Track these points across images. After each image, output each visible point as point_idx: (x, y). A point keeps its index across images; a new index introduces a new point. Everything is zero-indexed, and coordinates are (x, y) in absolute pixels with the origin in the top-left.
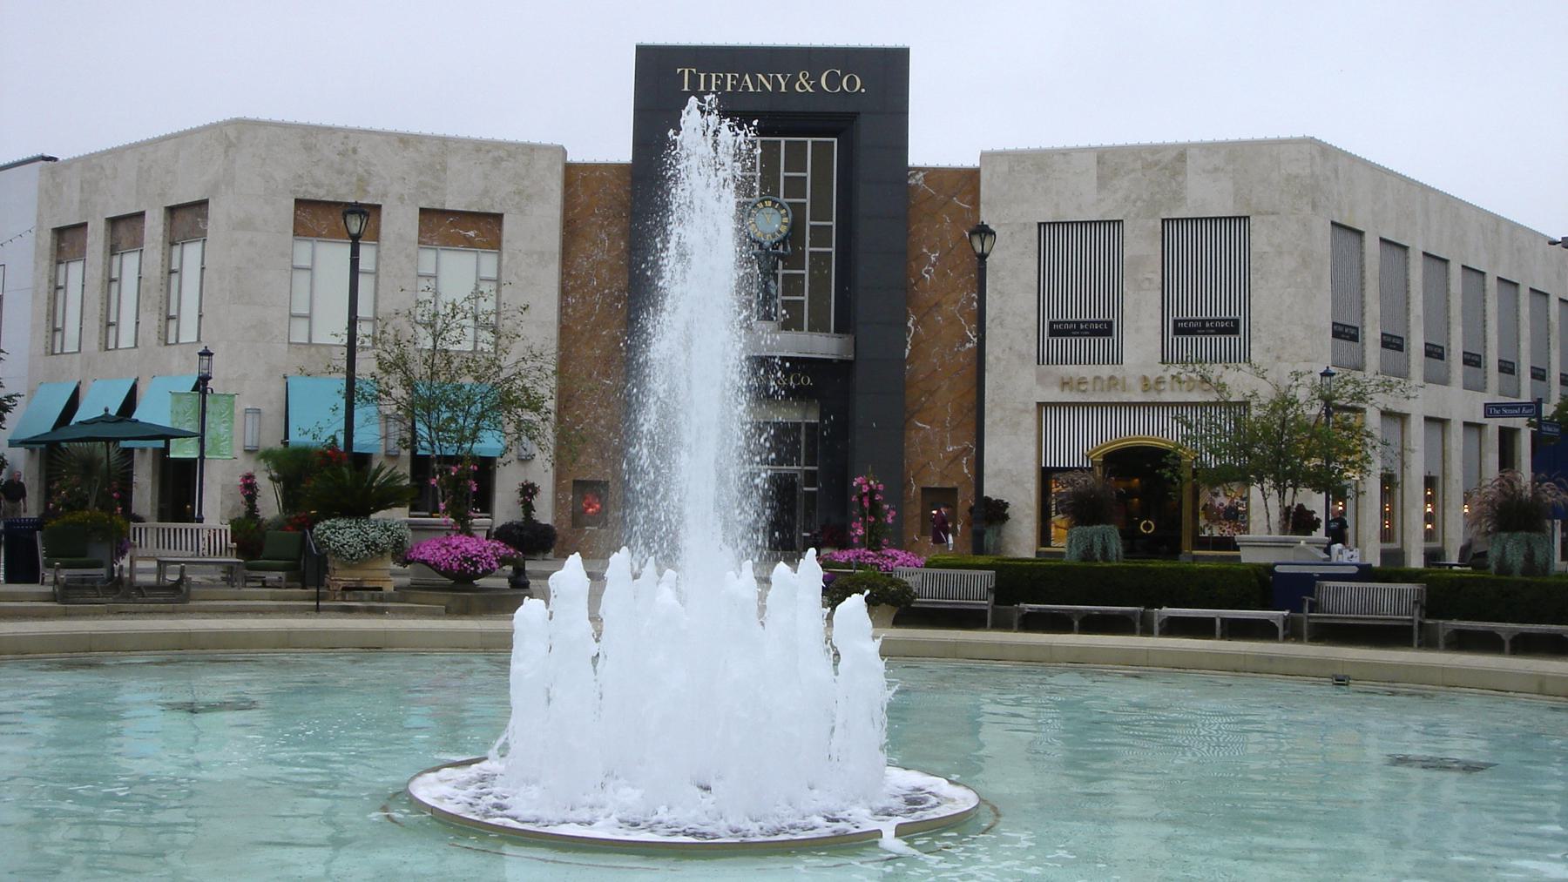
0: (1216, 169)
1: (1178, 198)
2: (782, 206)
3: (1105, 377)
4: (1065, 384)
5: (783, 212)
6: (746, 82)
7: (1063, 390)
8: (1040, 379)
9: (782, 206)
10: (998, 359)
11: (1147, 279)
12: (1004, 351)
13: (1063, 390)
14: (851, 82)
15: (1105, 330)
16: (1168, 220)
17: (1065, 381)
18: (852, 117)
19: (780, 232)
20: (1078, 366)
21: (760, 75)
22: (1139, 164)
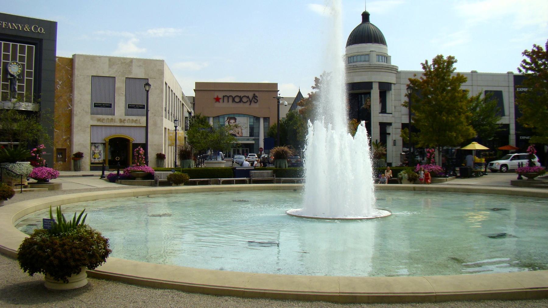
0: (140, 66)
1: (130, 72)
2: (19, 65)
3: (110, 119)
4: (99, 120)
5: (20, 66)
6: (9, 25)
8: (92, 119)
9: (19, 65)
10: (80, 113)
12: (81, 111)
14: (41, 30)
15: (109, 106)
16: (127, 78)
17: (99, 119)
18: (41, 40)
19: (18, 72)
21: (14, 24)
22: (120, 63)
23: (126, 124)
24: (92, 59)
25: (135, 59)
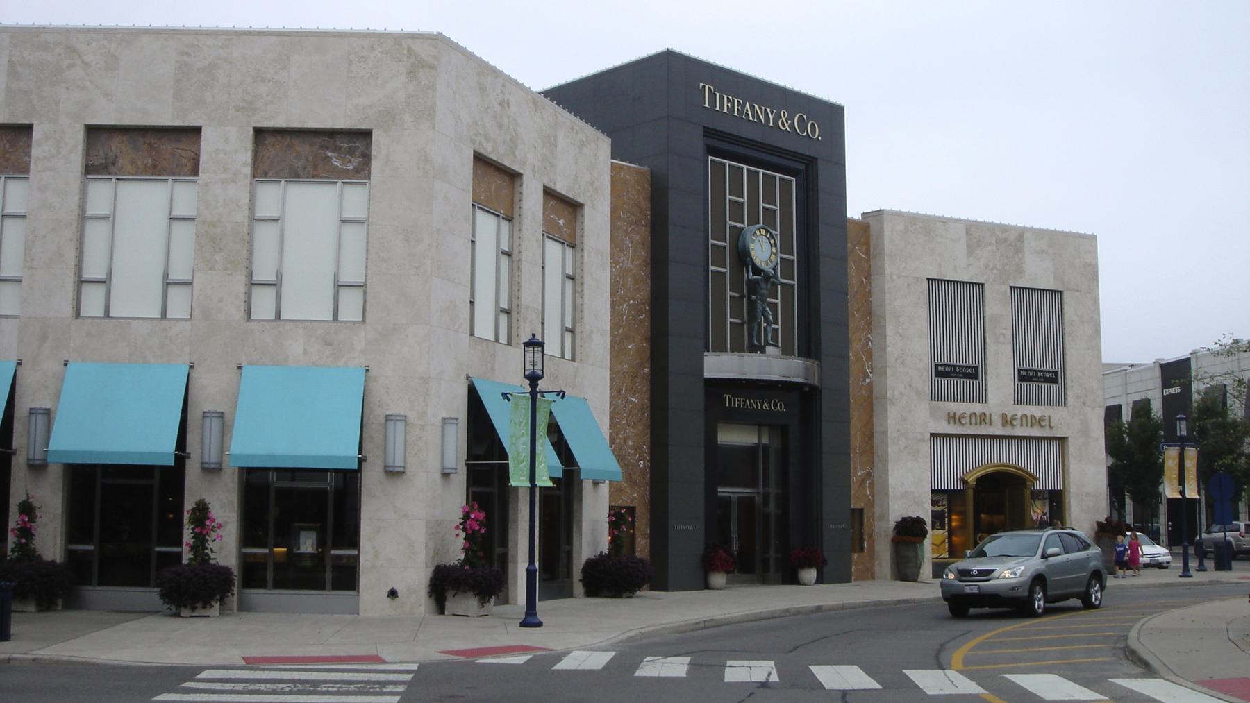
0: (1043, 251)
1: (1020, 271)
4: (952, 418)
7: (949, 423)
8: (933, 414)
11: (1003, 334)
12: (906, 387)
13: (949, 423)
20: (956, 403)
21: (756, 106)
22: (993, 241)
23: (1018, 432)
24: (925, 226)
25: (1031, 230)
